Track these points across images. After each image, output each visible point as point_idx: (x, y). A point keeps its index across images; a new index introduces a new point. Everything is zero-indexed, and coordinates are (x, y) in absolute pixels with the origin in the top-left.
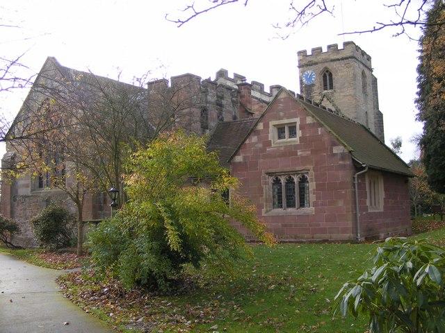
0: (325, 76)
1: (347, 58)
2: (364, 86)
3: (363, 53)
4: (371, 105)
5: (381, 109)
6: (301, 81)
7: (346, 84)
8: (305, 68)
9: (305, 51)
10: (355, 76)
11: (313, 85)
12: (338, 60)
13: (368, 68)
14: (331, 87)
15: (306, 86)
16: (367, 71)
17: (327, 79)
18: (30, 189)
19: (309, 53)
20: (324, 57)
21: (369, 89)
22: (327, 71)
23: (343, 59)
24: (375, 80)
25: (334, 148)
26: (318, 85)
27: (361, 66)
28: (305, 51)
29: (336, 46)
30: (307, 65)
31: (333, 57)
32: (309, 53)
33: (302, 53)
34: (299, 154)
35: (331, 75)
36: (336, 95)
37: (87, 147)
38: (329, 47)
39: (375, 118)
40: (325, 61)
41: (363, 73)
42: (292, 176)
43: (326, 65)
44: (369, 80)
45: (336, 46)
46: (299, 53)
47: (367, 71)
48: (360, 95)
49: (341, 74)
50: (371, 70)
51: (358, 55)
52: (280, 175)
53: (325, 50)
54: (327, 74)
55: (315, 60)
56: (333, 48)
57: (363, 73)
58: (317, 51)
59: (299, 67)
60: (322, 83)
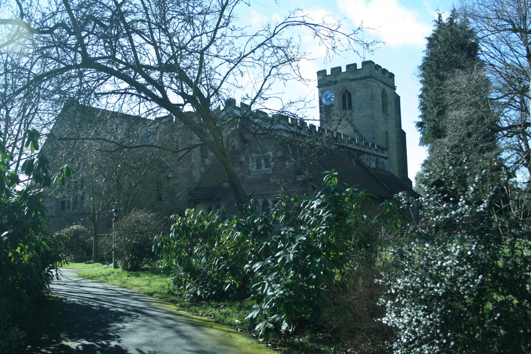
0: (344, 97)
1: (365, 78)
2: (384, 105)
3: (385, 71)
4: (392, 123)
5: (403, 128)
6: (321, 101)
7: (365, 105)
8: (325, 89)
9: (325, 71)
10: (373, 96)
11: (332, 105)
12: (356, 80)
13: (390, 87)
14: (350, 107)
15: (326, 106)
16: (388, 90)
17: (346, 100)
18: (54, 210)
19: (329, 73)
20: (343, 76)
21: (391, 108)
22: (346, 91)
23: (361, 79)
24: (398, 98)
25: (297, 176)
26: (337, 105)
27: (382, 85)
28: (325, 71)
29: (355, 65)
30: (326, 85)
31: (351, 77)
32: (329, 73)
33: (321, 73)
34: (272, 181)
35: (350, 95)
36: (355, 114)
37: (101, 181)
38: (348, 67)
39: (397, 137)
40: (344, 80)
41: (383, 91)
42: (267, 199)
43: (345, 84)
44: (391, 99)
45: (355, 65)
46: (319, 73)
47: (388, 90)
48: (379, 115)
49: (359, 94)
50: (394, 88)
51: (378, 73)
52: (268, 197)
53: (344, 70)
54: (346, 94)
55: (334, 79)
56: (352, 67)
57: (383, 91)
58: (336, 70)
59: (318, 87)
60: (341, 102)
